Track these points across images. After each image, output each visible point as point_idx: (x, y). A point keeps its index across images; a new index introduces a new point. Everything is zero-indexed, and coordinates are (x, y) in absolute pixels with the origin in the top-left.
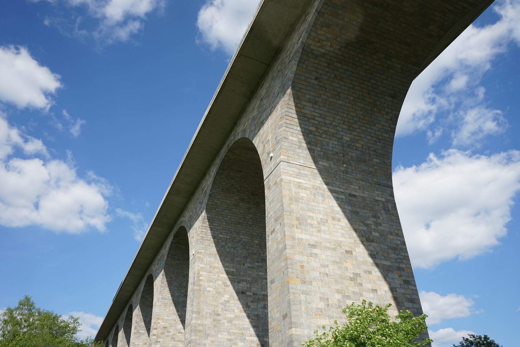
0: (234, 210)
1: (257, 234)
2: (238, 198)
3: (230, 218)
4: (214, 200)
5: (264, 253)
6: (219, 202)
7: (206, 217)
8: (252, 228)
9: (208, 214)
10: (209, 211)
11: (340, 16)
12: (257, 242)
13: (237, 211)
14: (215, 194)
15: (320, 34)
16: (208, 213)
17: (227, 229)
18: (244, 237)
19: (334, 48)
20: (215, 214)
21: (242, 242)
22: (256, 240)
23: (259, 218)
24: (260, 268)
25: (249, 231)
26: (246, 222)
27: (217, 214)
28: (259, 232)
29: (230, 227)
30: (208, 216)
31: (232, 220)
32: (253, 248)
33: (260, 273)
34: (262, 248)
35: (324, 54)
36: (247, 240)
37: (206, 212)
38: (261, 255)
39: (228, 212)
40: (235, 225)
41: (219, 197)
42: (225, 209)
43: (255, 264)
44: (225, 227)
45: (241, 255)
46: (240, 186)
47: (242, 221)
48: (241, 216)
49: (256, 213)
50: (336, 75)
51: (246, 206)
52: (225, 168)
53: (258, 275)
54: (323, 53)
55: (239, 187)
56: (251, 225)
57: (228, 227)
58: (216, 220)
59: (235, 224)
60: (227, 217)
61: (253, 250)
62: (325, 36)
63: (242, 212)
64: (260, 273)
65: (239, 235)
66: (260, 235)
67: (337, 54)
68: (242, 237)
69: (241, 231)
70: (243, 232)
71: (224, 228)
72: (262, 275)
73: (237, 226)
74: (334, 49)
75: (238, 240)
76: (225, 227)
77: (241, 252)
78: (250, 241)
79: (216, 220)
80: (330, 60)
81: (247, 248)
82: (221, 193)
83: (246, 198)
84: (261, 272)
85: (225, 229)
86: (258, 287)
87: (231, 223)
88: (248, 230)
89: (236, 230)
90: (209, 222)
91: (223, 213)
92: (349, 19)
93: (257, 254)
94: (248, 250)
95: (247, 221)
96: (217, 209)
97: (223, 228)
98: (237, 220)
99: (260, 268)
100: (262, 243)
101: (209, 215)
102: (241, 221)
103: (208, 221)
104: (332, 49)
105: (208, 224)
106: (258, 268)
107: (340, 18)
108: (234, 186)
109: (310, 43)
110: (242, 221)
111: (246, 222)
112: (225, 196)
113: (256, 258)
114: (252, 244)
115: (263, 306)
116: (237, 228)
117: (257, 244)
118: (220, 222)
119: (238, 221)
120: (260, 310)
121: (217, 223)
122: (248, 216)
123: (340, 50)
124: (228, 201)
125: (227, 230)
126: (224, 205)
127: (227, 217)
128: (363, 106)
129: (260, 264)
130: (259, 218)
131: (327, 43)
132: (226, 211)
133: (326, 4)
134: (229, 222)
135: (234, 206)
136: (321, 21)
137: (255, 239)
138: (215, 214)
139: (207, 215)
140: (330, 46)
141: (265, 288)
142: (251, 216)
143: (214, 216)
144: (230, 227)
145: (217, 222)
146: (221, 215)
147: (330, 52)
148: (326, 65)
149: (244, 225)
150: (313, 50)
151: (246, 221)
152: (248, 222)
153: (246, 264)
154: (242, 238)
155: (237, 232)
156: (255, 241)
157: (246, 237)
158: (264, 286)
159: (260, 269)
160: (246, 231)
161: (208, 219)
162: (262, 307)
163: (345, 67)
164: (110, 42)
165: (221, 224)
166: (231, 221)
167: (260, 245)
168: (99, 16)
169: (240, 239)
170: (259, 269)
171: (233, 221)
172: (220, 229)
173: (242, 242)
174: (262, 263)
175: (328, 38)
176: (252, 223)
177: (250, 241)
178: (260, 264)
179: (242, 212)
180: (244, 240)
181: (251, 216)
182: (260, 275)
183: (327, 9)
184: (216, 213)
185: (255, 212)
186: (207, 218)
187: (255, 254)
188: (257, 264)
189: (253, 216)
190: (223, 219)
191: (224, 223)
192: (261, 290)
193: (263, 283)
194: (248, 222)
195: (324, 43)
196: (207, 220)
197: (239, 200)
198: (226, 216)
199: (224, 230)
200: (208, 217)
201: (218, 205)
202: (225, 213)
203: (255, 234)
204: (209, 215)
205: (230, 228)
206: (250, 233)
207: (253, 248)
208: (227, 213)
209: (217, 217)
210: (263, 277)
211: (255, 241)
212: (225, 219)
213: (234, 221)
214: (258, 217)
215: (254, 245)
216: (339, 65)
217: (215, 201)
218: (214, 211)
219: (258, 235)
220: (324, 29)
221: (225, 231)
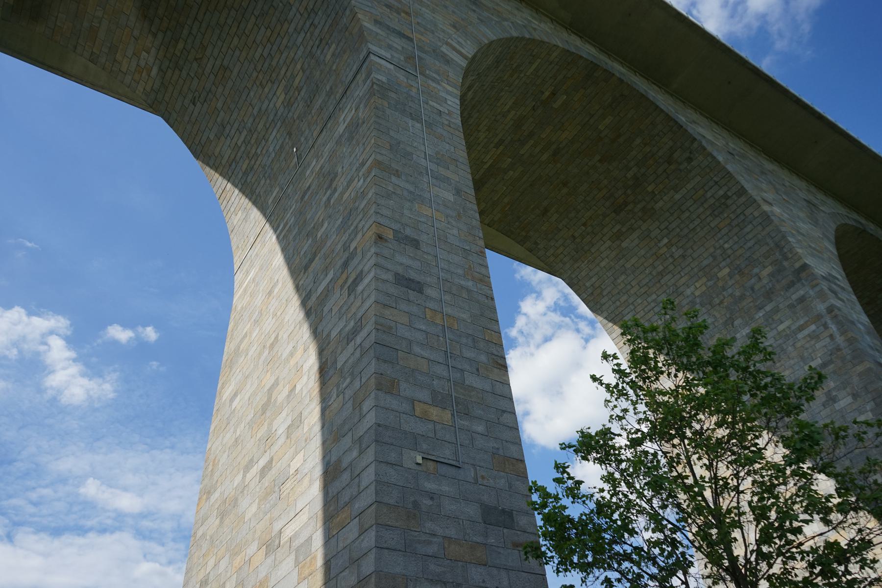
0: (628, 265)
1: (711, 259)
2: (609, 243)
3: (638, 284)
4: (584, 285)
5: (760, 278)
6: (594, 280)
7: (605, 320)
8: (690, 257)
9: (602, 313)
10: (598, 307)
11: (93, 24)
12: (726, 271)
13: (633, 261)
14: (573, 276)
15: (128, 67)
16: (600, 312)
17: (653, 305)
18: (692, 288)
19: (150, 46)
20: (611, 302)
21: (698, 300)
22: (721, 269)
23: (681, 230)
24: (774, 317)
25: (692, 269)
26: (671, 260)
27: (612, 299)
28: (712, 250)
29: (654, 297)
30: (605, 316)
31: (644, 282)
32: (730, 291)
33: (781, 327)
34: (746, 272)
35: (160, 69)
36: (704, 288)
37: (597, 314)
38: (756, 287)
39: (623, 277)
40: (658, 285)
41: (583, 274)
42: (615, 279)
43: (757, 317)
44: (646, 306)
45: (716, 325)
46: (584, 225)
47: (660, 266)
48: (651, 261)
49: (666, 228)
50: (196, 59)
51: (638, 237)
52: (524, 233)
53: (779, 333)
54: (158, 72)
55: (583, 228)
56: (683, 256)
57: (649, 300)
58: (621, 309)
59: (656, 283)
60: (632, 287)
61: (731, 295)
62: (131, 59)
63: (643, 252)
64: (781, 327)
65: (682, 293)
66: (719, 252)
67: (161, 44)
68: (688, 292)
69: (677, 284)
70: (683, 280)
71: (646, 309)
72: (789, 327)
73: (663, 282)
74: (153, 46)
75: (687, 304)
76: (646, 306)
77: (713, 320)
78: (710, 283)
79: (621, 309)
80: (170, 61)
81: (717, 301)
82: (576, 265)
83: (618, 227)
84: (782, 322)
85: (649, 307)
86: (792, 362)
87: (649, 288)
88: (686, 269)
89: (668, 291)
90: (615, 324)
91: (620, 288)
92: (98, 8)
93: (748, 294)
94: (721, 302)
95: (668, 256)
96: (605, 293)
97: (644, 311)
98: (650, 273)
99: (774, 317)
100: (738, 263)
101: (605, 314)
102: (661, 268)
103: (612, 323)
104: (153, 51)
105: (617, 328)
106: (770, 320)
107: (98, 25)
108: (576, 234)
109: (142, 90)
110: (660, 266)
111: (671, 260)
112: (589, 261)
113: (751, 304)
114: (720, 284)
115: (824, 399)
116: (664, 286)
117: (731, 276)
118: (631, 306)
119: (654, 273)
120: (821, 413)
121: (629, 313)
122: (660, 248)
123: (155, 35)
124: (603, 264)
125: (653, 306)
126: (605, 276)
127: (632, 287)
128: (253, 19)
129: (768, 308)
130: (681, 230)
131: (142, 57)
132: (619, 281)
133: (75, 47)
134: (643, 290)
135: (620, 259)
136: (106, 60)
137: (716, 270)
138: (611, 302)
139: (602, 316)
140: (148, 53)
141: (810, 351)
142: (666, 241)
143: (612, 307)
144: (654, 298)
145: (627, 312)
146: (622, 294)
147: (158, 57)
148: (177, 72)
149: (671, 267)
150: (154, 88)
151: (667, 258)
152: (672, 256)
153: (738, 336)
154: (693, 293)
155: (673, 292)
156: (720, 275)
157: (698, 285)
158: (807, 349)
159: (776, 318)
160: (686, 274)
161: (610, 321)
162: (824, 405)
163: (185, 32)
164: (806, 28)
165: (635, 307)
166: (645, 285)
167: (736, 272)
168: (756, 24)
169: (690, 299)
170: (773, 320)
171: (648, 283)
172: (642, 315)
173: (698, 300)
174: (772, 301)
175: (134, 54)
176: (681, 252)
177: (710, 283)
178: (768, 308)
179: (643, 252)
180: (697, 293)
181: (666, 241)
182: (784, 330)
183: (85, 47)
184: (610, 299)
185: (662, 227)
186: (607, 322)
187: (742, 297)
188: (761, 315)
189: (668, 239)
190: (630, 297)
191: (639, 301)
192: (802, 363)
193: (799, 345)
194: (672, 256)
195: (142, 63)
196: (610, 324)
197: (613, 242)
198: (629, 287)
199: (649, 312)
200: (606, 318)
201: (597, 285)
202: (623, 285)
203: (705, 263)
204: (605, 314)
205: (655, 299)
206: (696, 270)
207: (730, 291)
208: (623, 281)
209: (618, 303)
210: (793, 328)
211: (720, 275)
212: (632, 292)
213: (650, 280)
214: (678, 230)
215: (726, 282)
216: (180, 45)
217: (588, 284)
218: (604, 300)
219: (715, 258)
220: (119, 57)
221: (652, 311)
